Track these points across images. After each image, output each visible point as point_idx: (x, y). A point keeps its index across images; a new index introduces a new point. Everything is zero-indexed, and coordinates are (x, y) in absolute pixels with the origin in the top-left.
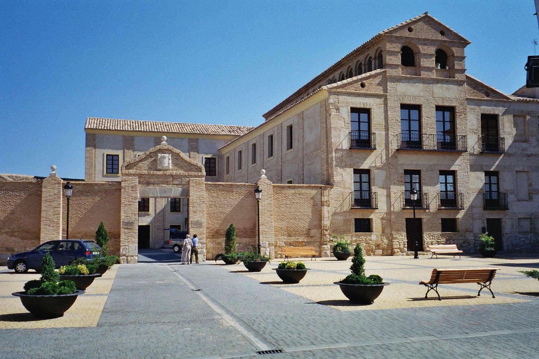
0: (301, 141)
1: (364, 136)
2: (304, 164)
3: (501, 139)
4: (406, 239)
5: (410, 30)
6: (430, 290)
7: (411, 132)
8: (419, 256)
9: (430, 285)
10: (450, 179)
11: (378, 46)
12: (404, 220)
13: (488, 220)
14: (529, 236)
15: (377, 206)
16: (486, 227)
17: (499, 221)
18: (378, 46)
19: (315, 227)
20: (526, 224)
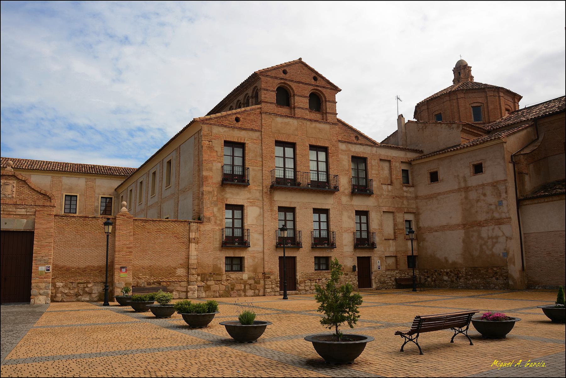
0: (178, 176)
1: (362, 183)
2: (179, 199)
3: (370, 180)
4: (279, 278)
5: (285, 72)
6: (408, 341)
7: (319, 172)
8: (288, 297)
9: (408, 336)
10: (323, 217)
11: (255, 85)
12: (278, 258)
13: (359, 258)
14: (395, 273)
15: (249, 244)
16: (356, 265)
17: (369, 258)
18: (255, 85)
19: (182, 266)
20: (391, 261)
